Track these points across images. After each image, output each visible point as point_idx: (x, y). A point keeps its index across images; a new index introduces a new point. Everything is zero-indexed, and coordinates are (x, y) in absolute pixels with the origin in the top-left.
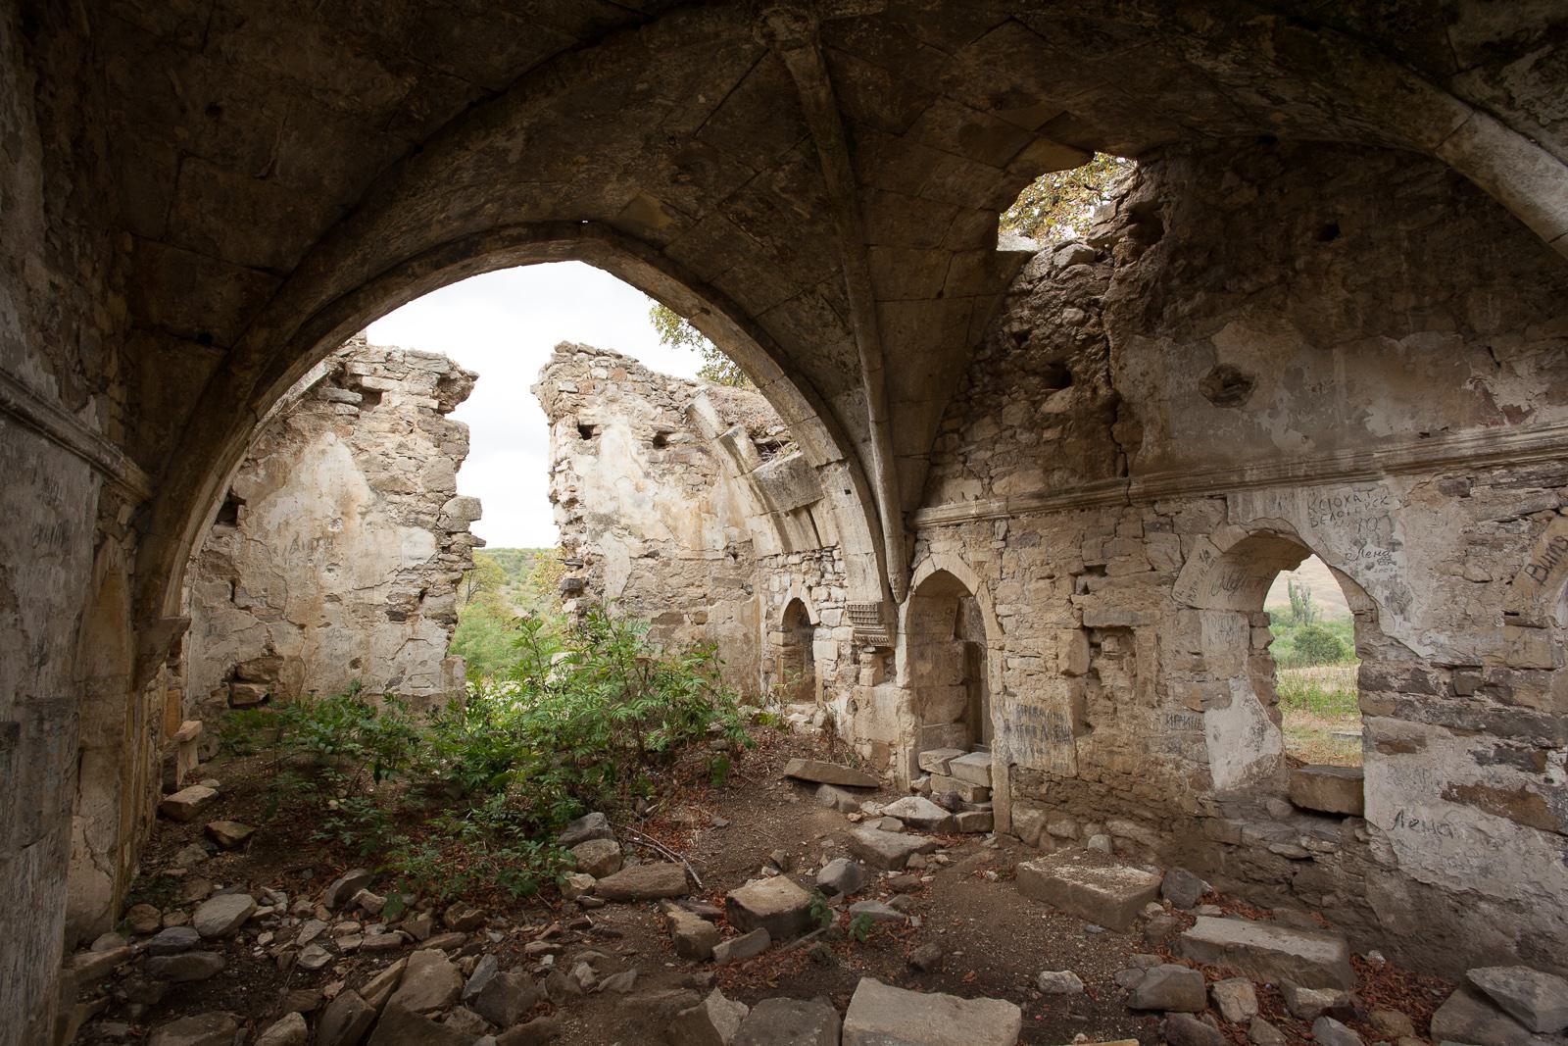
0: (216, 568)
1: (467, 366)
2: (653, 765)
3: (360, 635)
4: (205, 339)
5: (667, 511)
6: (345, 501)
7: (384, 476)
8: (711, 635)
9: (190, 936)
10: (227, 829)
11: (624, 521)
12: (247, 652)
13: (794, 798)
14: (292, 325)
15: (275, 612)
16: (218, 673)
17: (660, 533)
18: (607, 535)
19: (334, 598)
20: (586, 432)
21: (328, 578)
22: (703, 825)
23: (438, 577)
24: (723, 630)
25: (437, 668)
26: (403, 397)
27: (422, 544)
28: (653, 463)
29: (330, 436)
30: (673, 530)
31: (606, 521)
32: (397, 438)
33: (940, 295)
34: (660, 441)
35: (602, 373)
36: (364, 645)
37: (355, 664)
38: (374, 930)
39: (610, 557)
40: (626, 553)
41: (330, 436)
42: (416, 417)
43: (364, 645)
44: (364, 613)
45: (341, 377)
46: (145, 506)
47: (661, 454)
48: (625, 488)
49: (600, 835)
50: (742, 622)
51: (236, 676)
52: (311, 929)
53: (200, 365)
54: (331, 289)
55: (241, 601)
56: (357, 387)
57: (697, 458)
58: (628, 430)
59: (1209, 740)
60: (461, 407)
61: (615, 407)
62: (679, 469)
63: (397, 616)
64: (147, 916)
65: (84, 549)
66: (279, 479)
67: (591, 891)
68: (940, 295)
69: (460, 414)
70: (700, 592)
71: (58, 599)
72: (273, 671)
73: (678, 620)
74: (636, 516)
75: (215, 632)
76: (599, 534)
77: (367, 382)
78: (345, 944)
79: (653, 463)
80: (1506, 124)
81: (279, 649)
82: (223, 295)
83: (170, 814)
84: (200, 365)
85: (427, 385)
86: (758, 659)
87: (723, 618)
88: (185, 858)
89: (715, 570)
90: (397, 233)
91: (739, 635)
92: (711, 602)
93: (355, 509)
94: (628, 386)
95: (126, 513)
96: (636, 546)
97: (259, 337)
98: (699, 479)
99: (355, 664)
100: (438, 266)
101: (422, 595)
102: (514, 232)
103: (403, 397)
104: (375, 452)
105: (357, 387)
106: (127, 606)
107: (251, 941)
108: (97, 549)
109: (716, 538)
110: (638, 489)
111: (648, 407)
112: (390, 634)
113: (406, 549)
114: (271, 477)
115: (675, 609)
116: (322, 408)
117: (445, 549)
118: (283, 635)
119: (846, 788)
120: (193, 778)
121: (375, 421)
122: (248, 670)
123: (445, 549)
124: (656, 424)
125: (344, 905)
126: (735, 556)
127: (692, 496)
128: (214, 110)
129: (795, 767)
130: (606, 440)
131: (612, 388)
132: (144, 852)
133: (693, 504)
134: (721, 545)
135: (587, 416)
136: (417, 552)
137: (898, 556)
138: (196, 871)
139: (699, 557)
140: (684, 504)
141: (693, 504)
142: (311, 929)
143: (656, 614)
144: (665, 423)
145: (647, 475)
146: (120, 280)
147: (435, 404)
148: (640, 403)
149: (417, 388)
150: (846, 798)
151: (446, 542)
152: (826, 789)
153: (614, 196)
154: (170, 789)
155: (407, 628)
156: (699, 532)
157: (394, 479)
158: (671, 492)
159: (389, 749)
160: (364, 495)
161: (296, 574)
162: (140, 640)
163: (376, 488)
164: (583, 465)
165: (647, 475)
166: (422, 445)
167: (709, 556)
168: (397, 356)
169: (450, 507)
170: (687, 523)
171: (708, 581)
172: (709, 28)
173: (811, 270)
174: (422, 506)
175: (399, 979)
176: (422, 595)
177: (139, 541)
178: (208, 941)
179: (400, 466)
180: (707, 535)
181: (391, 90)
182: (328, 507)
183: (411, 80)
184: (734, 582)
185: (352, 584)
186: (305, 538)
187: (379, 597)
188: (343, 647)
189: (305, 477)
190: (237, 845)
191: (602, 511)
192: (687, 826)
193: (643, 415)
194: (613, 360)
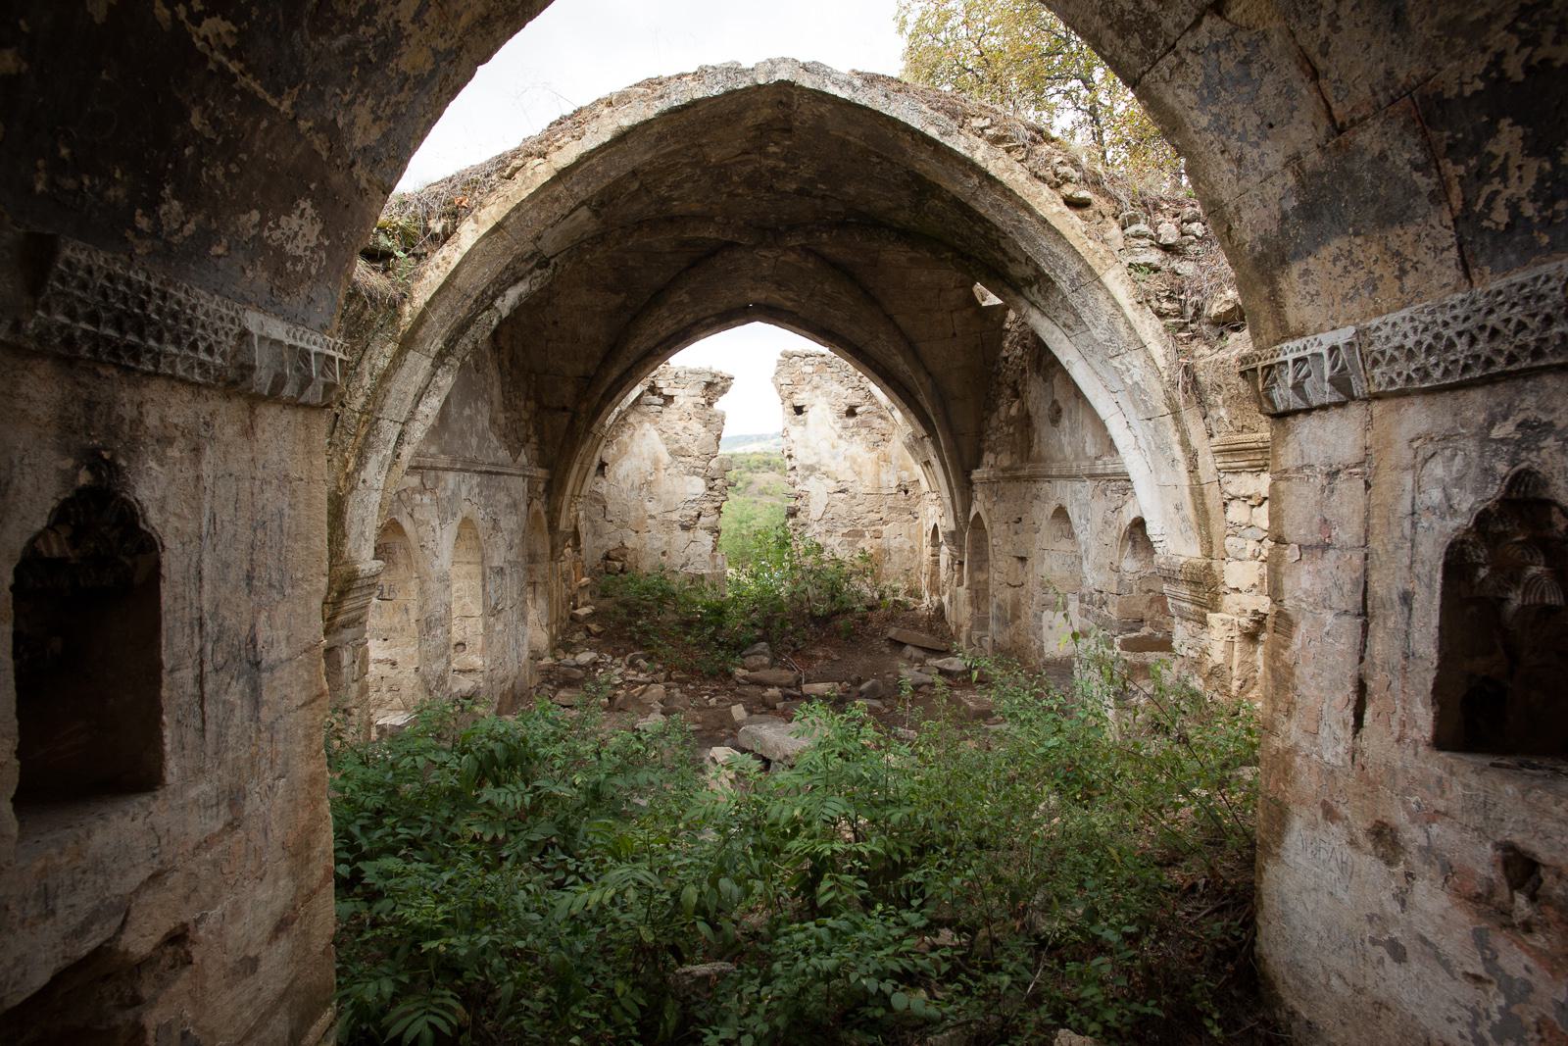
0: (596, 500)
1: (726, 372)
2: (817, 624)
3: (666, 538)
4: (564, 409)
5: (854, 461)
6: (656, 462)
7: (676, 446)
8: (886, 546)
9: (573, 663)
10: (594, 627)
11: (823, 469)
12: (612, 545)
13: (887, 650)
14: (596, 399)
15: (624, 524)
16: (600, 555)
17: (849, 476)
18: (812, 478)
19: (652, 517)
20: (799, 410)
21: (649, 505)
22: (825, 658)
23: (708, 505)
24: (894, 544)
25: (708, 559)
26: (686, 398)
27: (698, 486)
28: (845, 428)
29: (647, 425)
30: (859, 474)
31: (811, 469)
32: (682, 424)
33: (954, 335)
34: (851, 412)
35: (809, 369)
36: (668, 543)
37: (664, 553)
38: (642, 675)
39: (813, 492)
40: (824, 489)
41: (647, 425)
42: (692, 410)
43: (668, 543)
44: (668, 525)
45: (653, 389)
46: (549, 483)
47: (851, 421)
48: (825, 446)
49: (762, 653)
50: (910, 537)
51: (607, 557)
52: (618, 671)
53: (564, 420)
54: (610, 380)
55: (609, 518)
56: (661, 395)
57: (877, 423)
58: (827, 407)
59: (1045, 629)
60: (723, 399)
61: (818, 392)
62: (864, 431)
63: (685, 528)
64: (561, 654)
65: (523, 507)
66: (623, 452)
67: (745, 678)
68: (954, 335)
69: (721, 404)
70: (878, 516)
71: (515, 527)
72: (624, 555)
73: (862, 535)
74: (833, 466)
75: (597, 533)
76: (806, 478)
77: (665, 392)
78: (629, 678)
79: (845, 428)
80: (1044, 314)
81: (628, 544)
82: (569, 390)
83: (574, 618)
84: (564, 420)
85: (698, 390)
86: (920, 564)
87: (895, 535)
88: (578, 637)
89: (890, 501)
90: (639, 344)
91: (907, 547)
92: (886, 523)
93: (662, 466)
94: (827, 376)
95: (541, 488)
96: (832, 485)
97: (584, 406)
98: (880, 437)
99: (664, 553)
100: (670, 348)
101: (699, 515)
102: (708, 321)
103: (686, 398)
104: (671, 432)
105: (661, 395)
106: (546, 525)
107: (595, 670)
108: (528, 506)
109: (890, 479)
110: (833, 447)
111: (841, 389)
112: (681, 537)
113: (690, 489)
114: (619, 450)
115: (859, 527)
116: (645, 409)
117: (711, 489)
118: (628, 536)
119: (923, 649)
120: (585, 604)
121: (671, 414)
122: (613, 554)
123: (711, 489)
124: (847, 401)
125: (632, 665)
126: (906, 492)
127: (873, 450)
128: (555, 323)
129: (892, 632)
130: (811, 415)
131: (816, 379)
132: (563, 632)
133: (874, 455)
134: (894, 484)
135: (798, 401)
136: (696, 491)
137: (962, 500)
138: (580, 643)
139: (878, 492)
140: (867, 456)
141: (874, 455)
142: (618, 671)
143: (846, 531)
144: (855, 401)
145: (840, 437)
146: (532, 394)
147: (703, 401)
148: (836, 388)
149: (692, 393)
150: (920, 654)
151: (711, 485)
152: (908, 648)
153: (758, 295)
154: (575, 607)
155: (690, 535)
156: (878, 474)
157: (682, 448)
158: (858, 449)
159: (666, 596)
160: (666, 458)
161: (1460, 296)
162: (552, 540)
163: (672, 453)
164: (796, 432)
165: (840, 437)
166: (696, 427)
167: (885, 492)
168: (681, 374)
169: (713, 463)
170: (869, 469)
171: (884, 509)
172: (738, 256)
173: (1234, 131)
174: (699, 463)
175: (644, 691)
176: (699, 515)
177: (548, 497)
178: (578, 666)
179: (685, 440)
180: (884, 477)
181: (617, 300)
182: (647, 466)
183: (623, 295)
184: (904, 509)
185: (661, 509)
186: (637, 484)
187: (675, 516)
188: (657, 544)
189: (636, 450)
190: (598, 635)
191: (808, 462)
192: (817, 658)
193: (838, 396)
194: (819, 359)
